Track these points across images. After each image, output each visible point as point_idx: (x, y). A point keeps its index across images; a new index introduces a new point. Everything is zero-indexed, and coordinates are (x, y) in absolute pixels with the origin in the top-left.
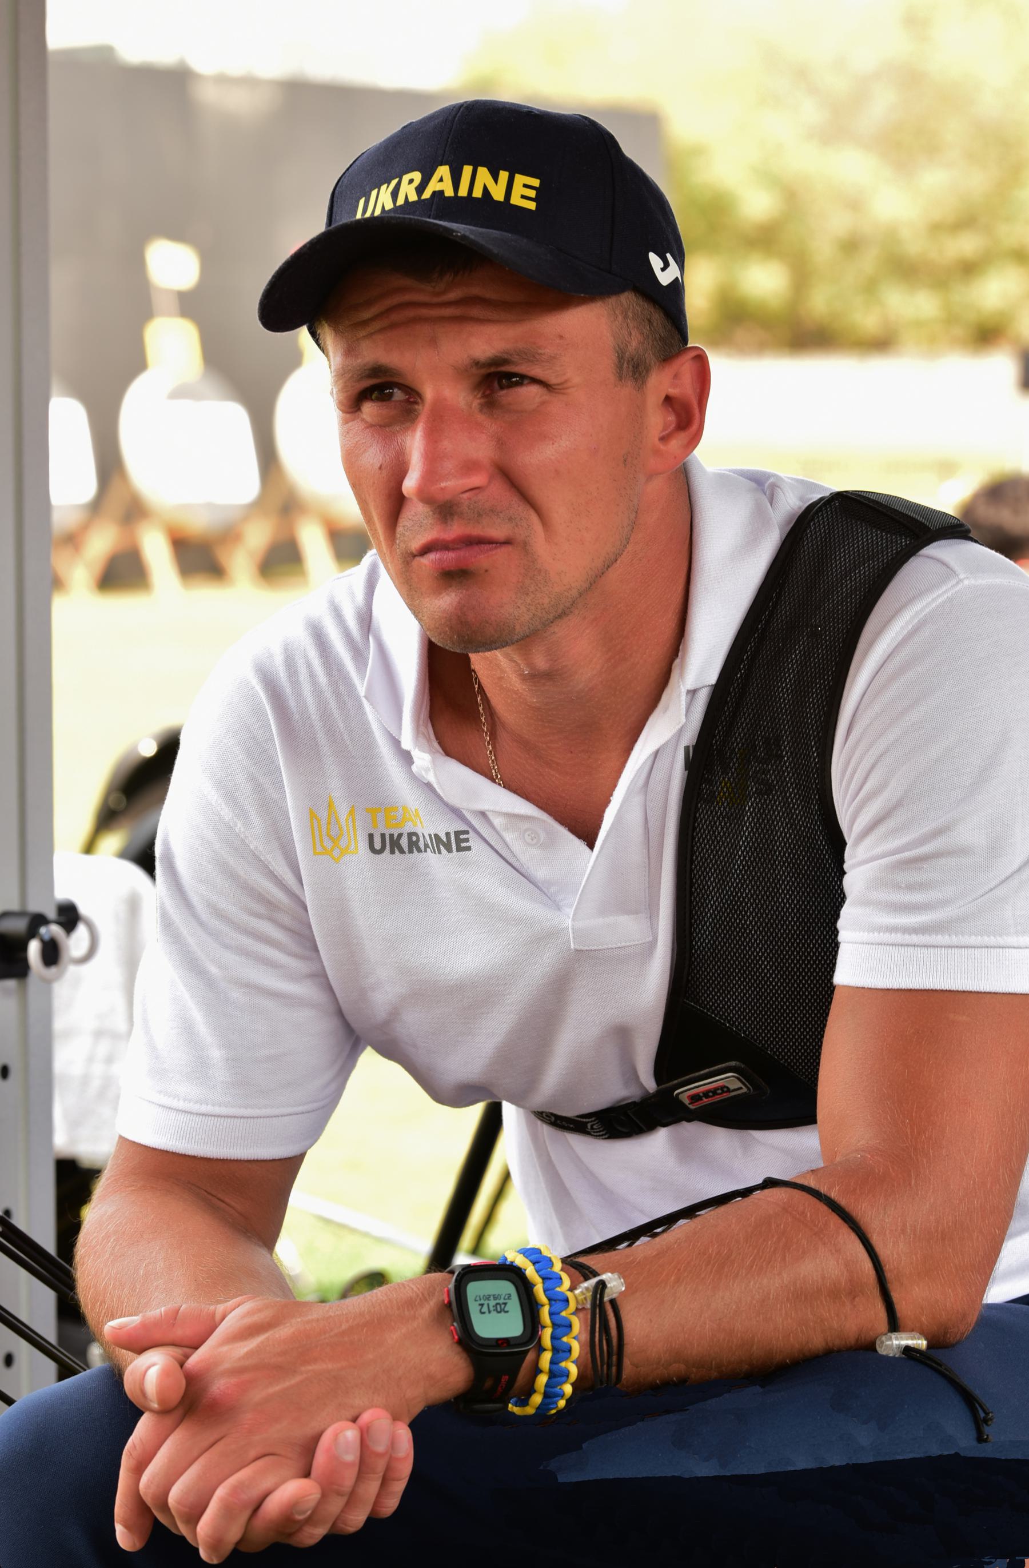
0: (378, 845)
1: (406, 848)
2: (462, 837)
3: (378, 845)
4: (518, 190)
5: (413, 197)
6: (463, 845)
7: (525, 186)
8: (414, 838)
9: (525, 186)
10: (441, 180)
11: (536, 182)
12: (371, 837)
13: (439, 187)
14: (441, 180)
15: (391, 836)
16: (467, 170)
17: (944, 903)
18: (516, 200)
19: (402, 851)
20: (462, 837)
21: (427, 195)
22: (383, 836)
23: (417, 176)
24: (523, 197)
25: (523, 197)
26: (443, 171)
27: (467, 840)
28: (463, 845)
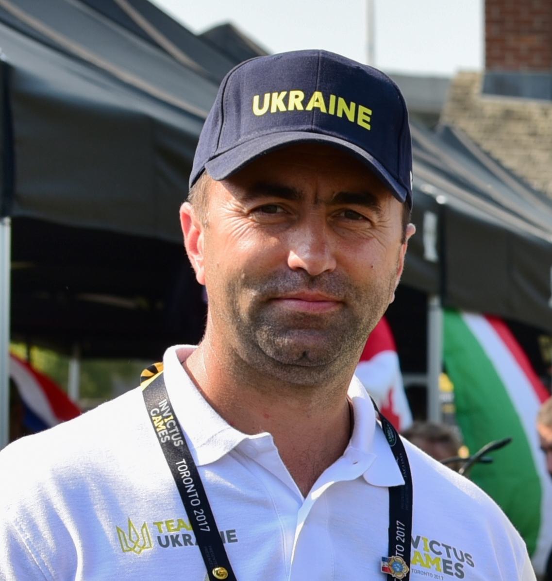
0: (164, 543)
1: (182, 542)
2: (231, 534)
3: (164, 543)
4: (361, 117)
5: (300, 107)
6: (232, 539)
7: (365, 114)
8: (187, 538)
9: (365, 114)
10: (317, 101)
11: (369, 112)
12: (159, 538)
13: (316, 105)
14: (317, 101)
15: (172, 537)
16: (267, 96)
17: (282, 529)
18: (360, 123)
19: (180, 545)
20: (231, 534)
21: (309, 108)
22: (166, 537)
23: (301, 95)
24: (364, 121)
25: (364, 121)
26: (318, 95)
27: (234, 536)
28: (232, 539)
